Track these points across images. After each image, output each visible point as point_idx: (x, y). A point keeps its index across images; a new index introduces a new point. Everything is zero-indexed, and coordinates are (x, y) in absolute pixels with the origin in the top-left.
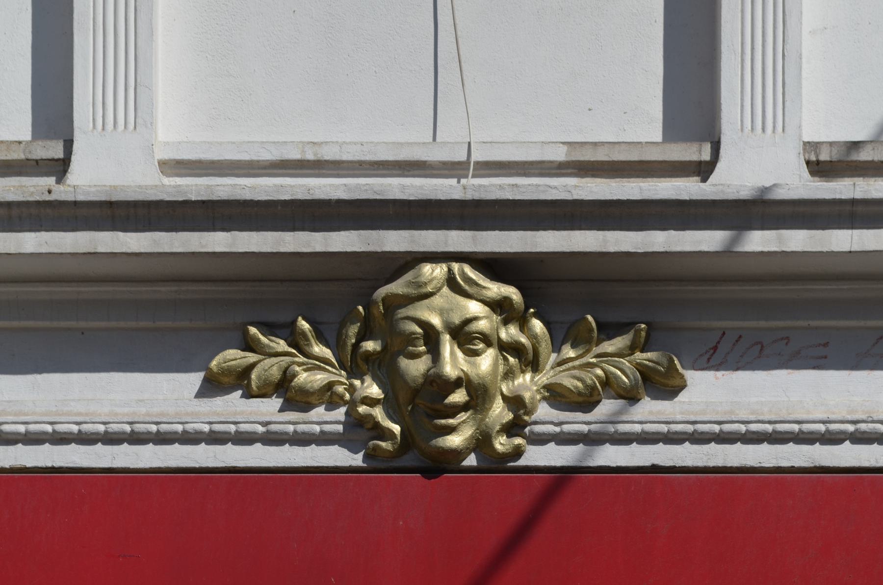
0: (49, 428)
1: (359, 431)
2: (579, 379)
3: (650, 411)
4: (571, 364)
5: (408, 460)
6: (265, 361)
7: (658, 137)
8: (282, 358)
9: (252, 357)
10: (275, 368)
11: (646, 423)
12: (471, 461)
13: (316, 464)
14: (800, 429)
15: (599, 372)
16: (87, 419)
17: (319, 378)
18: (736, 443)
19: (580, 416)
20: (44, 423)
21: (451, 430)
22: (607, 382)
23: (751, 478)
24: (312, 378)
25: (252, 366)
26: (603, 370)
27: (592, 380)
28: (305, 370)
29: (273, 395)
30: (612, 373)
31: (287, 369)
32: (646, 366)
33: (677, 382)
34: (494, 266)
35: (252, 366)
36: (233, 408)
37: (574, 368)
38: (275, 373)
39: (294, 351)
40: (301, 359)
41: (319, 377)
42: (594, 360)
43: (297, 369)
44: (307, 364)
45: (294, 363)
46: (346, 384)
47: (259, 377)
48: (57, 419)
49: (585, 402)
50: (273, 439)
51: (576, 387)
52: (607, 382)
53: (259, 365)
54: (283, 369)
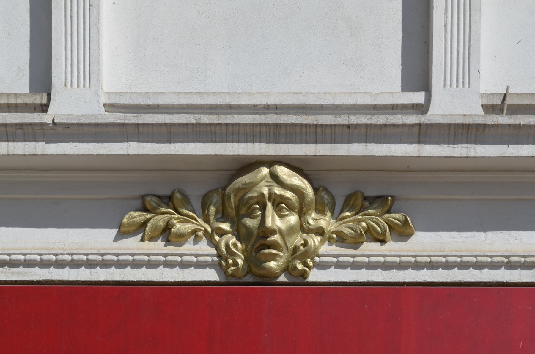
0: (38, 258)
1: (222, 260)
2: (352, 229)
3: (393, 247)
4: (348, 219)
5: (249, 279)
6: (156, 217)
7: (27, 90)
8: (164, 216)
9: (148, 216)
10: (161, 221)
11: (528, 256)
12: (283, 278)
13: (392, 281)
14: (525, 261)
15: (364, 224)
16: (46, 252)
17: (188, 227)
18: (453, 268)
19: (351, 251)
20: (49, 254)
21: (273, 257)
22: (369, 230)
23: (261, 288)
24: (183, 227)
25: (148, 220)
26: (366, 223)
27: (360, 230)
28: (180, 222)
29: (159, 237)
30: (372, 226)
31: (169, 221)
32: (392, 222)
33: (408, 231)
34: (296, 165)
35: (148, 220)
36: (133, 244)
37: (347, 222)
38: (162, 224)
39: (171, 211)
40: (177, 216)
41: (187, 226)
42: (361, 217)
43: (175, 222)
44: (179, 218)
45: (171, 218)
46: (202, 230)
47: (152, 225)
48: (42, 252)
49: (355, 242)
50: (340, 266)
51: (351, 233)
52: (369, 230)
53: (152, 220)
54: (167, 221)
